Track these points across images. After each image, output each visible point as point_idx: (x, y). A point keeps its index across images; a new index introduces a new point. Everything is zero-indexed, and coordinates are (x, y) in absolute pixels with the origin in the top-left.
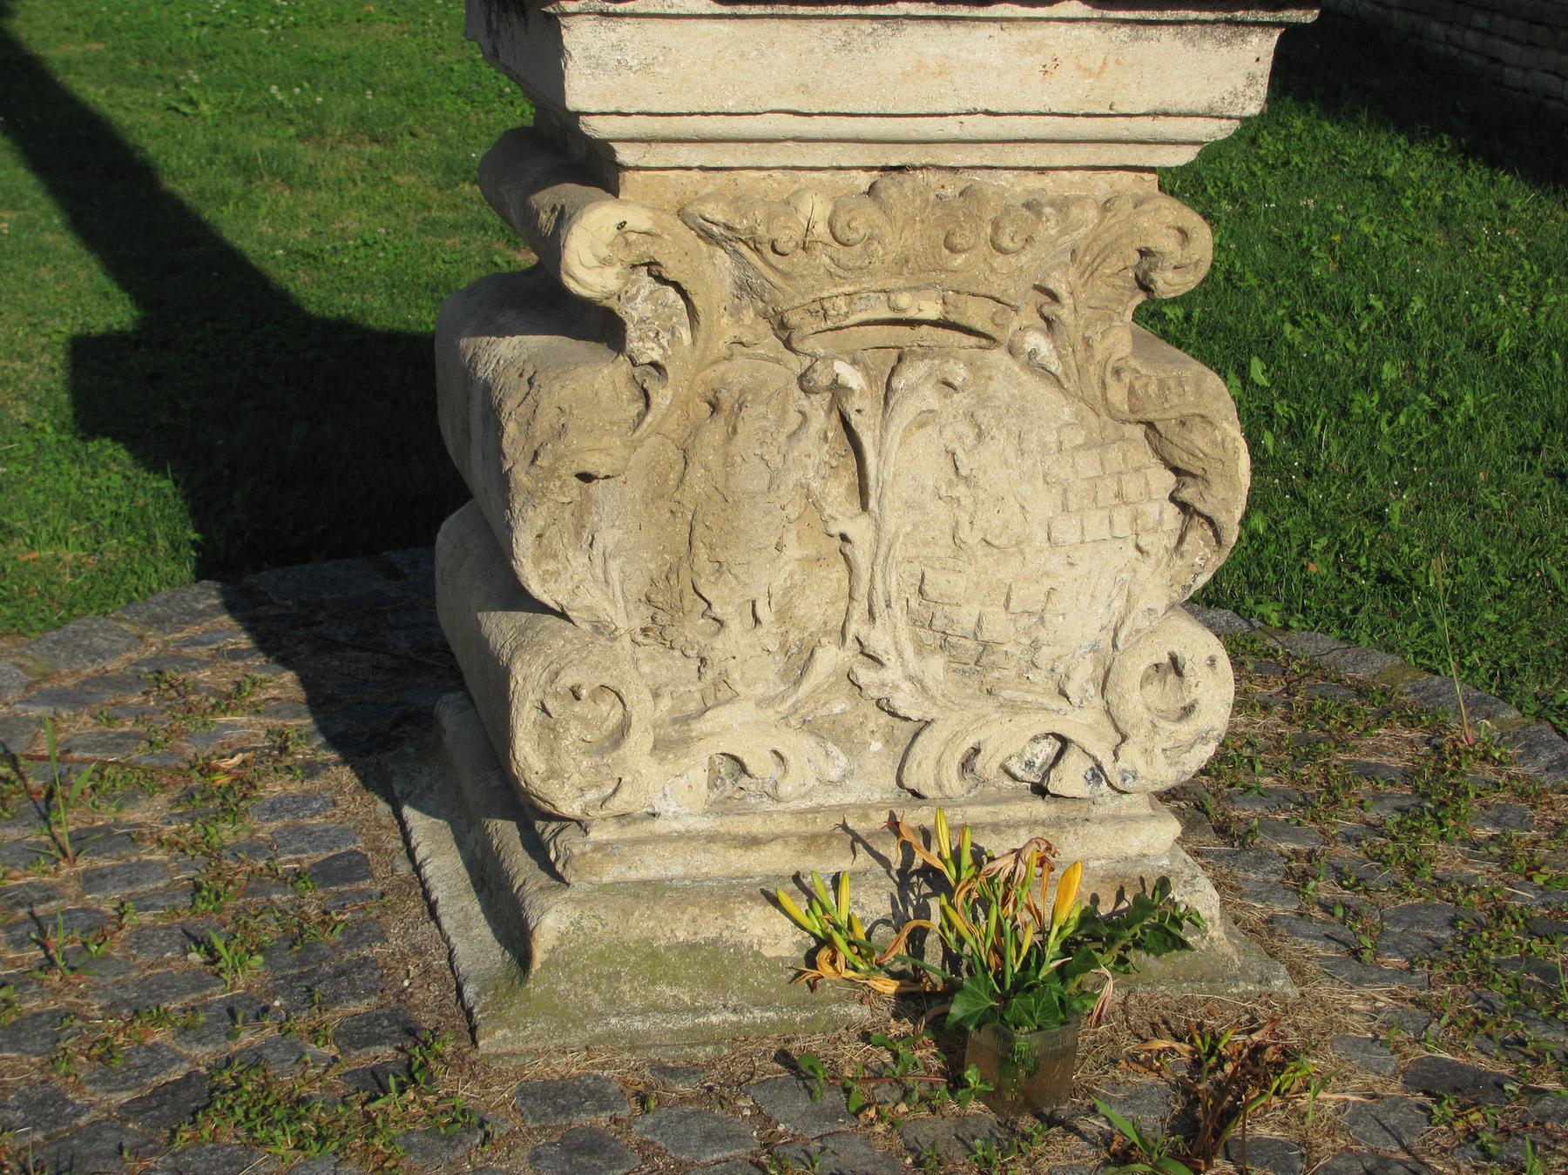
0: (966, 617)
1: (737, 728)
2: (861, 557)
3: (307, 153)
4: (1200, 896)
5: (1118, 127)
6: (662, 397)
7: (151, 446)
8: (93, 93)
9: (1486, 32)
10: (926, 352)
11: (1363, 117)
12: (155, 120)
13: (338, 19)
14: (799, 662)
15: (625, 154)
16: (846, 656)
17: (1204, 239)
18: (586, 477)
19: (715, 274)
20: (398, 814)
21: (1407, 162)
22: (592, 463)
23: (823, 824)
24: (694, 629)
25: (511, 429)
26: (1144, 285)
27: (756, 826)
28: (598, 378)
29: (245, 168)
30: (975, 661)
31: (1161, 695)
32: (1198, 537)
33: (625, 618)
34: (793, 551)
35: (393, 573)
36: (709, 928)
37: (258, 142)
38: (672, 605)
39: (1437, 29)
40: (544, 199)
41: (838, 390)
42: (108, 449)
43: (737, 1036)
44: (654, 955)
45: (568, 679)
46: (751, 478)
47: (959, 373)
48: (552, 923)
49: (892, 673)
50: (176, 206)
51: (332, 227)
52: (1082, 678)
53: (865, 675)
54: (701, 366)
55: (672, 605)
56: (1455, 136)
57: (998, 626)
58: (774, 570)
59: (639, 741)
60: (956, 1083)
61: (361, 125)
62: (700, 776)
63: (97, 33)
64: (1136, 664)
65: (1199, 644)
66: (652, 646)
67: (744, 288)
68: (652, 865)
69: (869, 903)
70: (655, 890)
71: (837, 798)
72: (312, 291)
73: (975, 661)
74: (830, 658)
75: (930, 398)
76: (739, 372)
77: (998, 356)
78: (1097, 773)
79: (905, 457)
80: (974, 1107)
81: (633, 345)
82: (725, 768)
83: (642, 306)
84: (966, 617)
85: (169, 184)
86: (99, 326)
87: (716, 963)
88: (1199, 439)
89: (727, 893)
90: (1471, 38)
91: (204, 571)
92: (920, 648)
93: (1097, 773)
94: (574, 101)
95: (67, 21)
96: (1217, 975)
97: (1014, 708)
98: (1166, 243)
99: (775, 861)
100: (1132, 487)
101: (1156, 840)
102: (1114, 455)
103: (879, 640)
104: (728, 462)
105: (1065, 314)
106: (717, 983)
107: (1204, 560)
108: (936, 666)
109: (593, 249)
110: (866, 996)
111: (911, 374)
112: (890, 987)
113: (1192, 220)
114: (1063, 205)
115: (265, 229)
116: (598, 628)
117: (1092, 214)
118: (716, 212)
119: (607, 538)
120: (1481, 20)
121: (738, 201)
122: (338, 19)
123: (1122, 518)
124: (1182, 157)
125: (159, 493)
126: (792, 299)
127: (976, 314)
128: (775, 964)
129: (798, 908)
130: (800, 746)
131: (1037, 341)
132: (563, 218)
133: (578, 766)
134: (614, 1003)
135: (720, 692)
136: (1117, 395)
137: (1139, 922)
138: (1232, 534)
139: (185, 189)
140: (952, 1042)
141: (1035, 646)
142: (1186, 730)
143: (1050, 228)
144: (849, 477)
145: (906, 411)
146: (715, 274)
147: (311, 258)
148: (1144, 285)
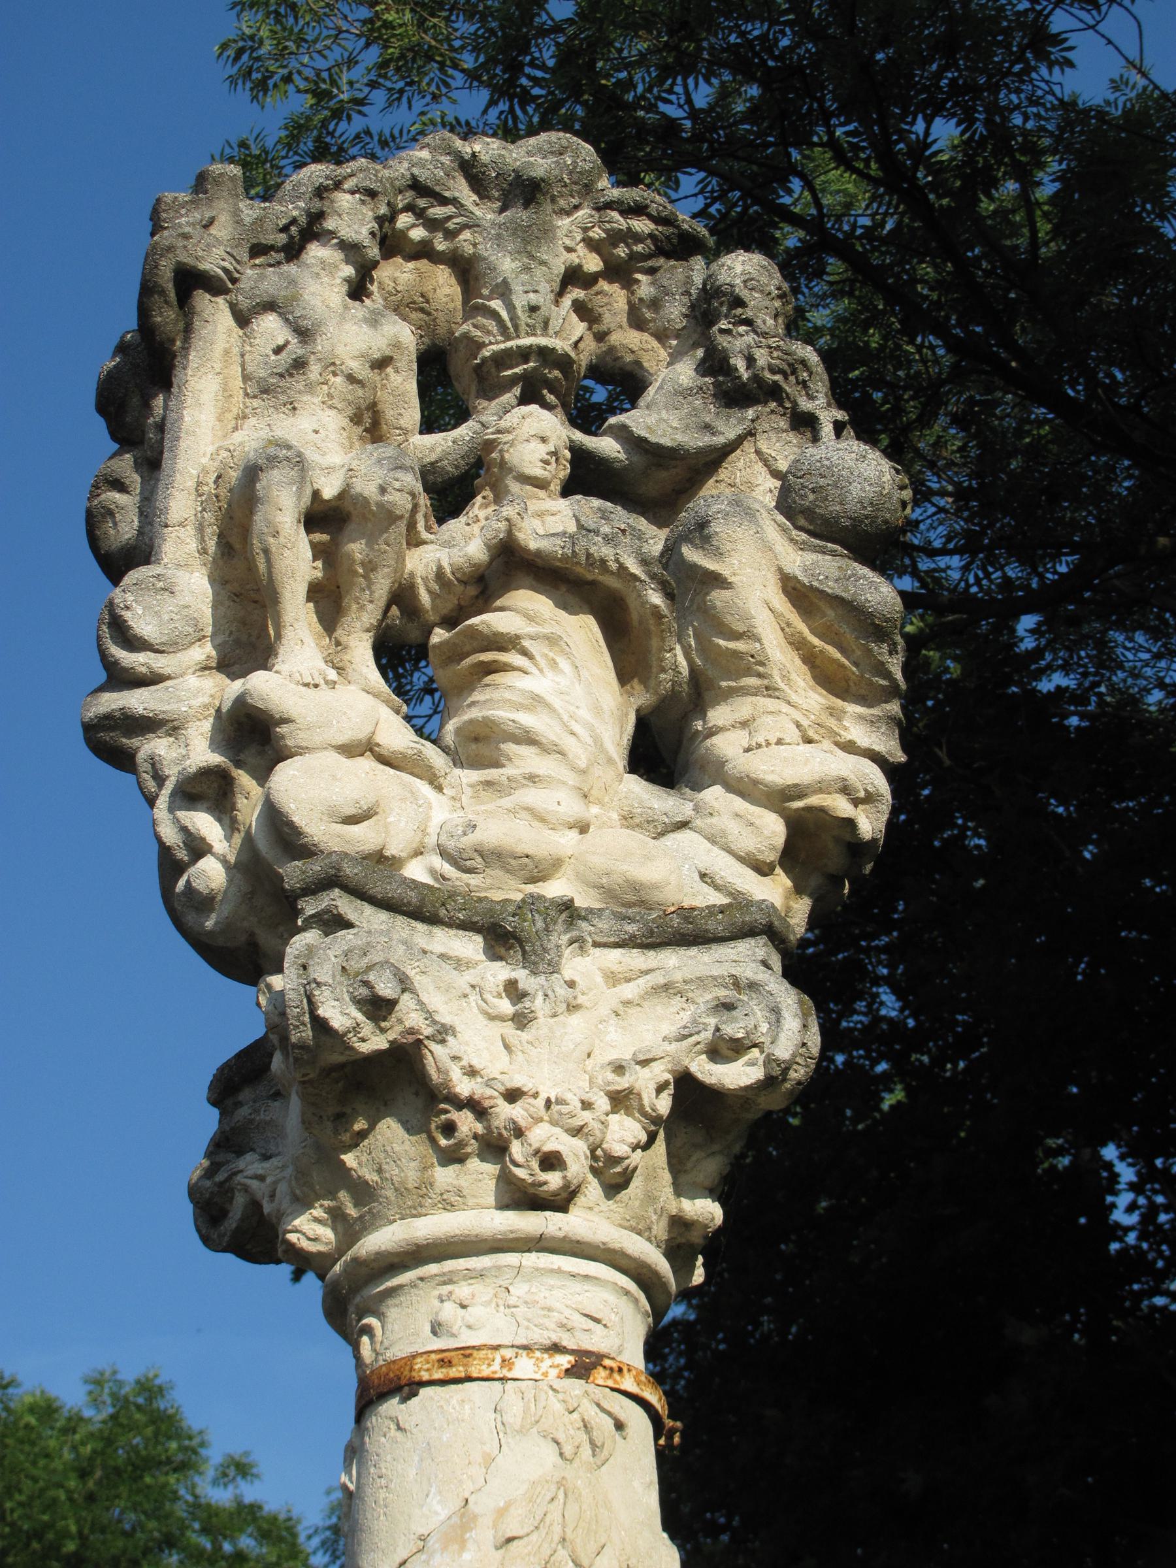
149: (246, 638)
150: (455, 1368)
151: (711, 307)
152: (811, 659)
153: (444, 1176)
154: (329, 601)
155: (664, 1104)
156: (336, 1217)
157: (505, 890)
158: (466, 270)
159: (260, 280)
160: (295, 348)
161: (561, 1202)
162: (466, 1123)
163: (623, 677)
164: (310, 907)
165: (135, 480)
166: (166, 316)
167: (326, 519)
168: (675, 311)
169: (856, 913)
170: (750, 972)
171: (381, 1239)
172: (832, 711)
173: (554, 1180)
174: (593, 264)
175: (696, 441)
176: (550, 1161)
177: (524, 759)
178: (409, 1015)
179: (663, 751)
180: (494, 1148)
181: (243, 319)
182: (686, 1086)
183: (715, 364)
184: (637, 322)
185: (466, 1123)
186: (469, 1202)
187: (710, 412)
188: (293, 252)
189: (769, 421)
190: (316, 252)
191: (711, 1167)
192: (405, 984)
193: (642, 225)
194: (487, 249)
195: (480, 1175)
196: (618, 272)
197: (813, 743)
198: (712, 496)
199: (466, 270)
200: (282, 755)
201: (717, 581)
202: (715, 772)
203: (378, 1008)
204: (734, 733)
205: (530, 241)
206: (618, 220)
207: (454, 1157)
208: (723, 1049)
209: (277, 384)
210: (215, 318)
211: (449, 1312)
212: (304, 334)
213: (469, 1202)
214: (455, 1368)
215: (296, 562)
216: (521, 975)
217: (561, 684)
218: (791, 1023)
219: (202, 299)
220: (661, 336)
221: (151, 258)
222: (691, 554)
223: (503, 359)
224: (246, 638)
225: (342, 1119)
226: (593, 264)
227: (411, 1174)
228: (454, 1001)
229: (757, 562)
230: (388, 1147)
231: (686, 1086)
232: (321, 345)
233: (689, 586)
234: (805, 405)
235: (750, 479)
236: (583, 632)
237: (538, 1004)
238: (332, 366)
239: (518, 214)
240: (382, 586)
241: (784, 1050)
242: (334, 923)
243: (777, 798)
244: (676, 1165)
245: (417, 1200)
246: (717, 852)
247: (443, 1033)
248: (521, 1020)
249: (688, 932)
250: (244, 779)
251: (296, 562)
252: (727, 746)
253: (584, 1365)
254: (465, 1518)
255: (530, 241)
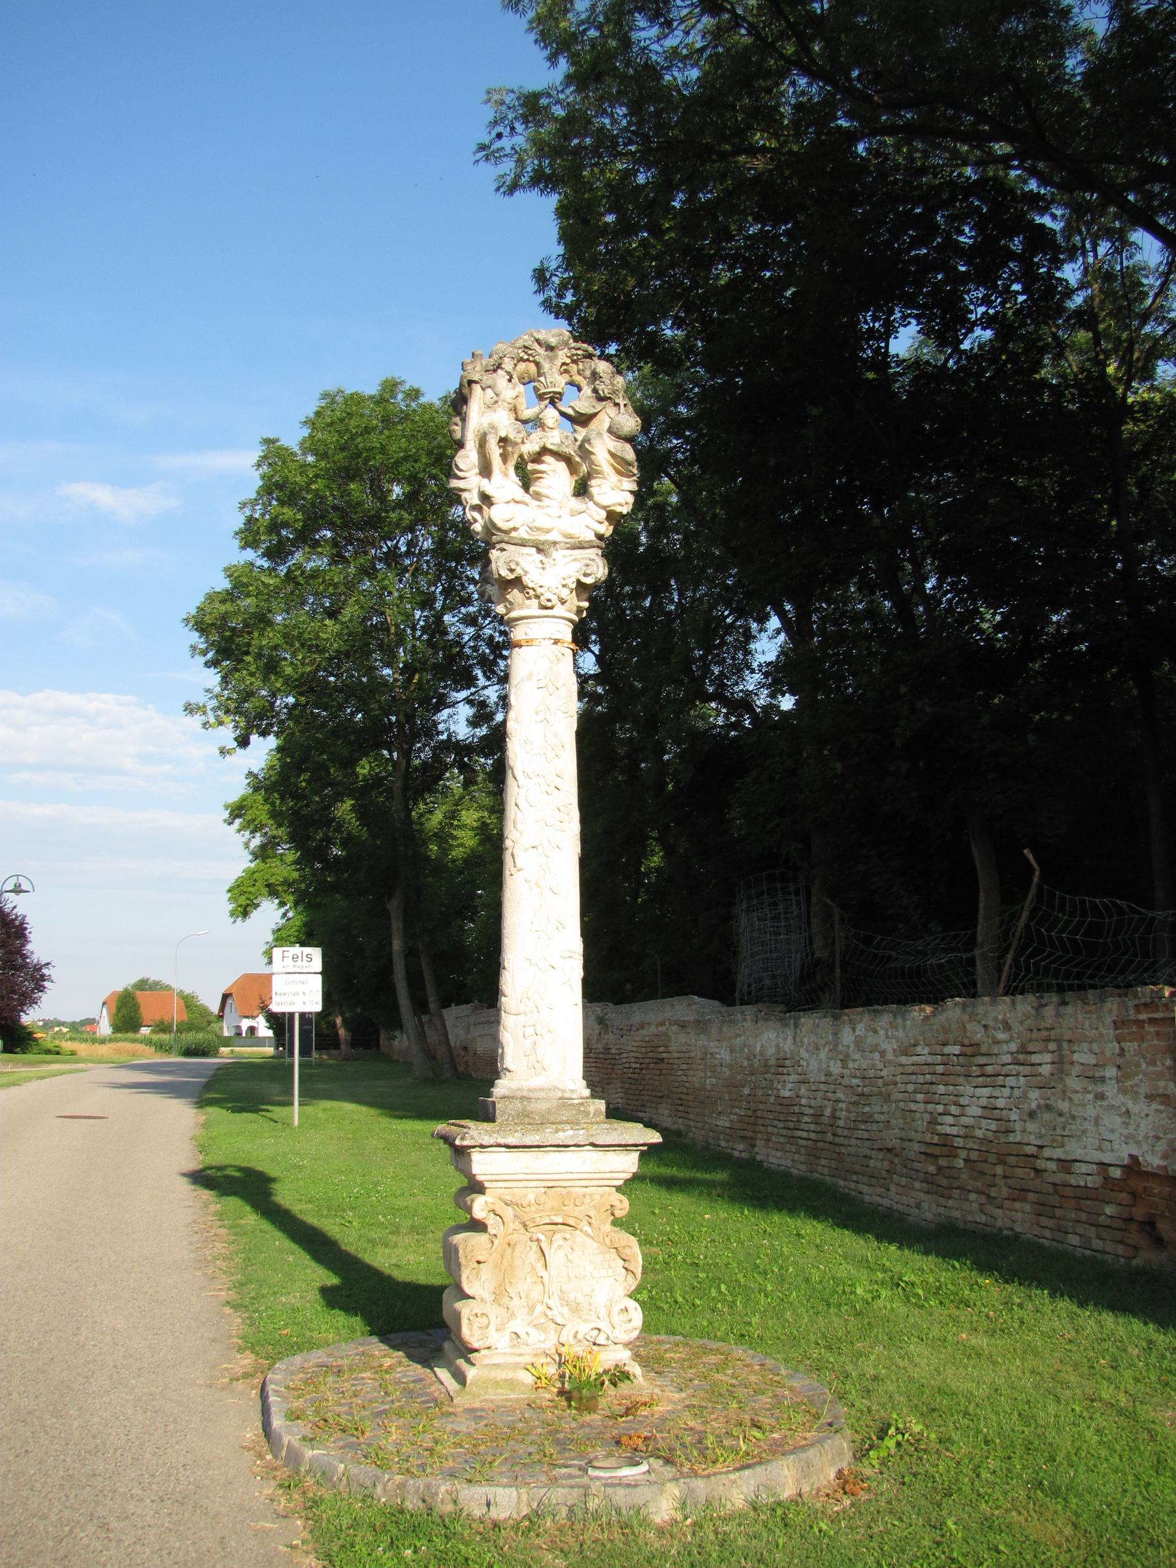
0: (572, 1296)
1: (516, 1325)
2: (546, 1280)
3: (394, 1238)
4: (635, 1369)
5: (602, 1176)
6: (496, 1242)
7: (349, 1310)
8: (312, 1220)
9: (857, 1182)
10: (560, 1231)
11: (802, 1214)
12: (337, 1229)
13: (402, 1195)
14: (531, 1309)
15: (487, 1184)
16: (544, 1308)
17: (626, 1202)
18: (479, 1262)
19: (508, 1213)
20: (434, 1373)
21: (812, 1229)
22: (481, 1258)
23: (539, 1351)
24: (506, 1300)
25: (461, 1251)
26: (613, 1214)
27: (522, 1351)
28: (480, 1239)
29: (372, 1242)
30: (576, 1308)
31: (624, 1317)
32: (630, 1276)
33: (489, 1297)
34: (529, 1280)
35: (429, 1335)
36: (510, 1375)
37: (376, 1234)
38: (500, 1295)
39: (841, 1183)
40: (468, 1198)
41: (538, 1240)
42: (337, 1311)
43: (517, 1400)
44: (497, 1382)
45: (475, 1311)
46: (518, 1262)
47: (568, 1236)
48: (471, 1373)
49: (555, 1312)
50: (348, 1254)
51: (404, 1259)
52: (603, 1312)
53: (548, 1312)
54: (506, 1236)
55: (500, 1295)
56: (833, 1219)
57: (580, 1299)
58: (523, 1285)
59: (492, 1327)
60: (570, 1406)
61: (413, 1229)
62: (507, 1337)
63: (310, 1202)
64: (616, 1310)
65: (632, 1305)
66: (496, 1305)
67: (516, 1216)
68: (496, 1360)
69: (552, 1370)
70: (497, 1365)
71: (543, 1346)
72: (399, 1275)
73: (576, 1308)
74: (540, 1308)
75: (561, 1242)
76: (515, 1237)
77: (578, 1232)
78: (608, 1338)
79: (555, 1257)
80: (574, 1411)
81: (490, 1230)
82: (514, 1336)
83: (491, 1221)
84: (572, 1296)
85: (344, 1248)
86: (329, 1284)
87: (512, 1384)
88: (628, 1251)
89: (516, 1366)
90: (852, 1185)
91: (372, 1333)
92: (562, 1305)
93: (608, 1338)
94: (474, 1172)
95: (298, 1197)
96: (641, 1388)
97: (585, 1321)
98: (617, 1203)
99: (528, 1359)
100: (613, 1264)
101: (623, 1355)
102: (608, 1256)
103: (551, 1304)
104: (512, 1258)
105: (593, 1221)
106: (513, 1389)
107: (633, 1284)
108: (565, 1310)
109: (480, 1207)
110: (550, 1392)
111: (557, 1236)
112: (556, 1390)
113: (624, 1198)
114: (591, 1195)
115: (381, 1259)
116: (482, 1300)
117: (598, 1197)
118: (508, 1198)
119: (484, 1277)
120: (855, 1177)
121: (514, 1195)
122: (402, 1195)
123: (610, 1271)
124: (621, 1182)
125: (357, 1321)
126: (526, 1218)
127: (571, 1221)
128: (527, 1385)
129: (533, 1370)
130: (533, 1332)
131: (587, 1228)
132: (472, 1201)
133: (477, 1333)
134: (486, 1393)
135: (513, 1316)
136: (607, 1241)
137: (620, 1376)
138: (639, 1276)
139: (351, 1249)
140: (569, 1399)
141: (590, 1304)
142: (630, 1326)
143: (588, 1200)
144: (542, 1262)
145: (555, 1245)
146: (508, 1213)
147: (396, 1265)
148: (613, 1214)
149: (486, 470)
150: (529, 642)
151: (595, 376)
152: (615, 469)
153: (527, 602)
154: (505, 457)
155: (574, 586)
156: (506, 607)
157: (543, 537)
158: (537, 364)
159: (487, 379)
160: (495, 398)
161: (552, 608)
162: (531, 592)
163: (571, 474)
164: (498, 546)
165: (460, 423)
166: (465, 391)
167: (504, 441)
168: (588, 373)
169: (618, 547)
170: (593, 557)
171: (513, 614)
172: (620, 481)
173: (549, 604)
174: (568, 361)
175: (591, 411)
176: (549, 600)
177: (546, 502)
178: (519, 571)
179: (582, 490)
180: (537, 597)
181: (483, 389)
182: (579, 583)
183: (595, 391)
184: (579, 374)
185: (531, 592)
186: (532, 608)
187: (595, 402)
188: (495, 371)
189: (609, 404)
190: (500, 371)
191: (586, 596)
192: (517, 564)
193: (580, 352)
194: (542, 361)
195: (535, 602)
196: (574, 362)
197: (616, 492)
198: (594, 424)
199: (537, 364)
200: (492, 504)
201: (592, 453)
202: (591, 498)
203: (512, 571)
204: (596, 487)
205: (552, 360)
206: (574, 352)
207: (529, 598)
208: (586, 575)
209: (492, 406)
210: (477, 389)
211: (528, 631)
212: (497, 395)
213: (532, 608)
214: (529, 642)
215: (495, 451)
216: (543, 558)
217: (556, 478)
218: (601, 569)
219: (474, 385)
220: (585, 378)
221: (462, 377)
222: (587, 446)
223: (545, 394)
224: (486, 470)
225: (506, 589)
226: (568, 361)
227: (520, 601)
228: (527, 564)
229: (603, 448)
230: (515, 595)
231: (579, 583)
232: (501, 397)
233: (585, 452)
234: (617, 401)
235: (602, 423)
236: (562, 466)
237: (547, 566)
238: (504, 401)
239: (550, 354)
240: (516, 456)
241: (599, 576)
242: (503, 550)
243: (604, 508)
244: (578, 596)
245: (522, 607)
246: (590, 523)
247: (526, 573)
248: (543, 569)
249: (581, 546)
250: (485, 507)
251: (495, 451)
252: (594, 490)
253: (556, 642)
254: (531, 675)
255: (552, 360)
